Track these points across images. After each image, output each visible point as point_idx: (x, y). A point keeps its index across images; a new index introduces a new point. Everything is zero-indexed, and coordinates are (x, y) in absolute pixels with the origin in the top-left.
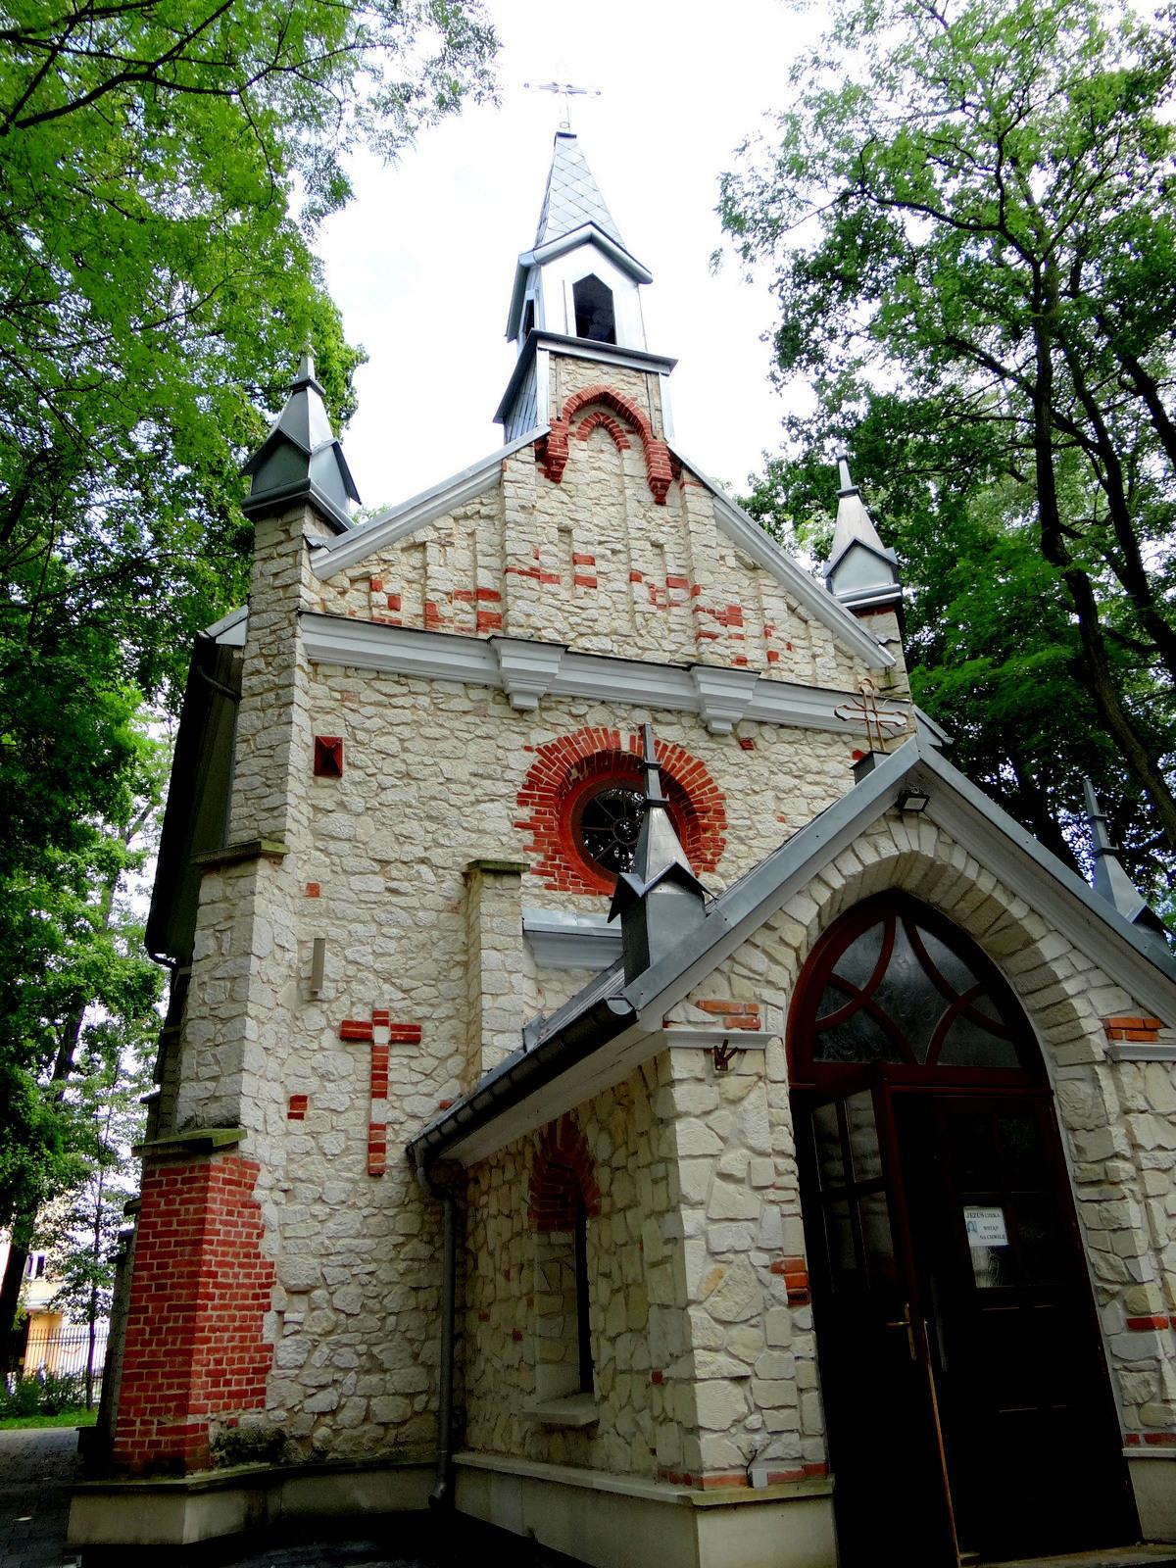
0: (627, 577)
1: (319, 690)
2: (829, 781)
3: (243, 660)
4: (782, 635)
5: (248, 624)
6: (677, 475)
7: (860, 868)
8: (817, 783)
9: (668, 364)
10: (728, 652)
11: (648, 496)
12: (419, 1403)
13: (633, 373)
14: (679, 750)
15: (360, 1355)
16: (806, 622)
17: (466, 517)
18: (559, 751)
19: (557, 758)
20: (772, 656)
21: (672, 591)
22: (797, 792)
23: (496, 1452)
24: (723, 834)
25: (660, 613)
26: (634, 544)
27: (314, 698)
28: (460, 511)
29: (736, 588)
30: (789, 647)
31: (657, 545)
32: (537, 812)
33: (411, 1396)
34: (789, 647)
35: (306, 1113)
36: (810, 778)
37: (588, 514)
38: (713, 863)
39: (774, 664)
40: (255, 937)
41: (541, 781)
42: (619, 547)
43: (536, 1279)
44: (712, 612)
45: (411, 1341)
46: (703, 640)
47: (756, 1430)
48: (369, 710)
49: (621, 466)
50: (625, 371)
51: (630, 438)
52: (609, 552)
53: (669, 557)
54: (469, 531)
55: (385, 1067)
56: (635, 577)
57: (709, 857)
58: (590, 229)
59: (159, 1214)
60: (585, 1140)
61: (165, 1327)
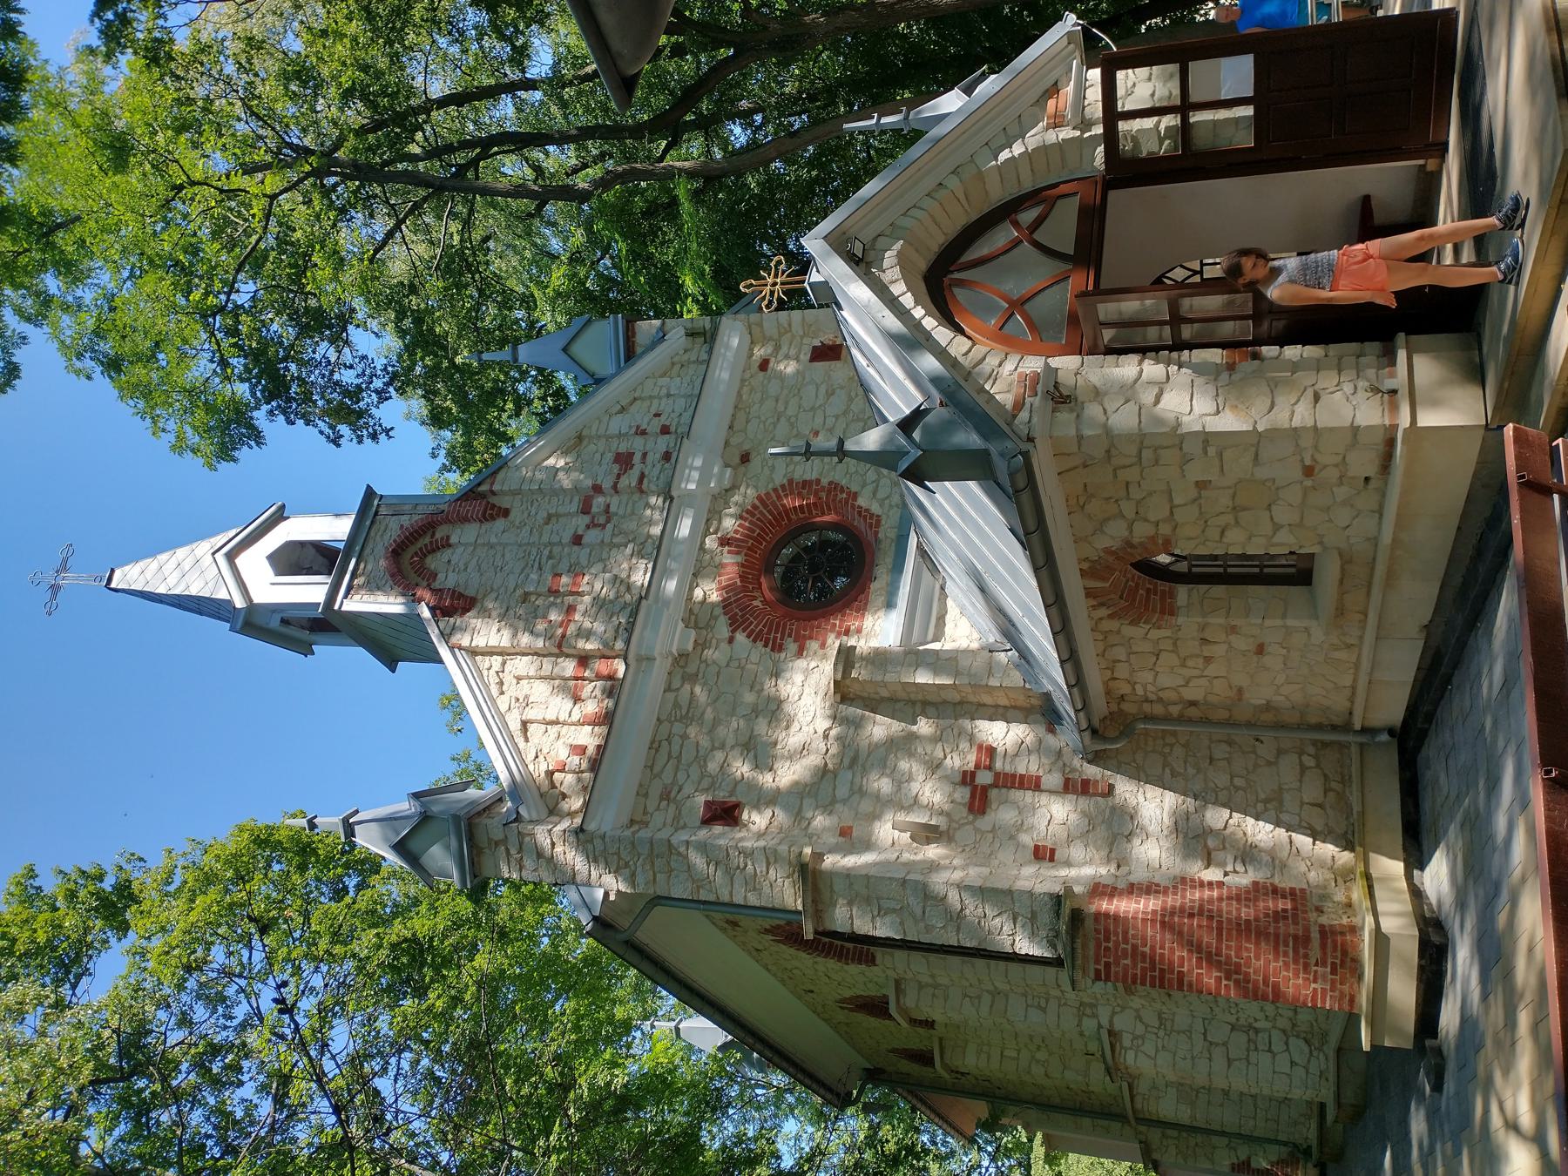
0: (576, 548)
1: (657, 819)
2: (785, 392)
3: (618, 891)
4: (646, 420)
5: (583, 885)
6: (483, 496)
7: (909, 294)
8: (787, 403)
9: (370, 493)
10: (659, 466)
11: (500, 523)
12: (1309, 762)
13: (375, 527)
14: (745, 515)
15: (1266, 810)
16: (635, 399)
17: (501, 683)
18: (736, 614)
19: (742, 617)
20: (665, 430)
21: (594, 509)
22: (793, 419)
23: (1355, 680)
24: (825, 482)
25: (615, 520)
26: (545, 539)
27: (664, 825)
28: (494, 690)
29: (598, 456)
30: (657, 415)
31: (549, 517)
32: (790, 636)
33: (1303, 769)
34: (657, 415)
35: (1050, 846)
36: (781, 408)
37: (511, 576)
38: (849, 494)
39: (673, 429)
40: (888, 875)
41: (761, 630)
42: (546, 552)
43: (1217, 620)
44: (619, 476)
45: (1256, 766)
46: (644, 486)
47: (1356, 387)
48: (681, 776)
49: (466, 545)
50: (372, 533)
51: (438, 535)
52: (550, 562)
53: (561, 510)
54: (515, 681)
55: (1014, 776)
56: (577, 540)
57: (844, 496)
58: (220, 557)
59: (1135, 966)
60: (1108, 551)
61: (1234, 959)
